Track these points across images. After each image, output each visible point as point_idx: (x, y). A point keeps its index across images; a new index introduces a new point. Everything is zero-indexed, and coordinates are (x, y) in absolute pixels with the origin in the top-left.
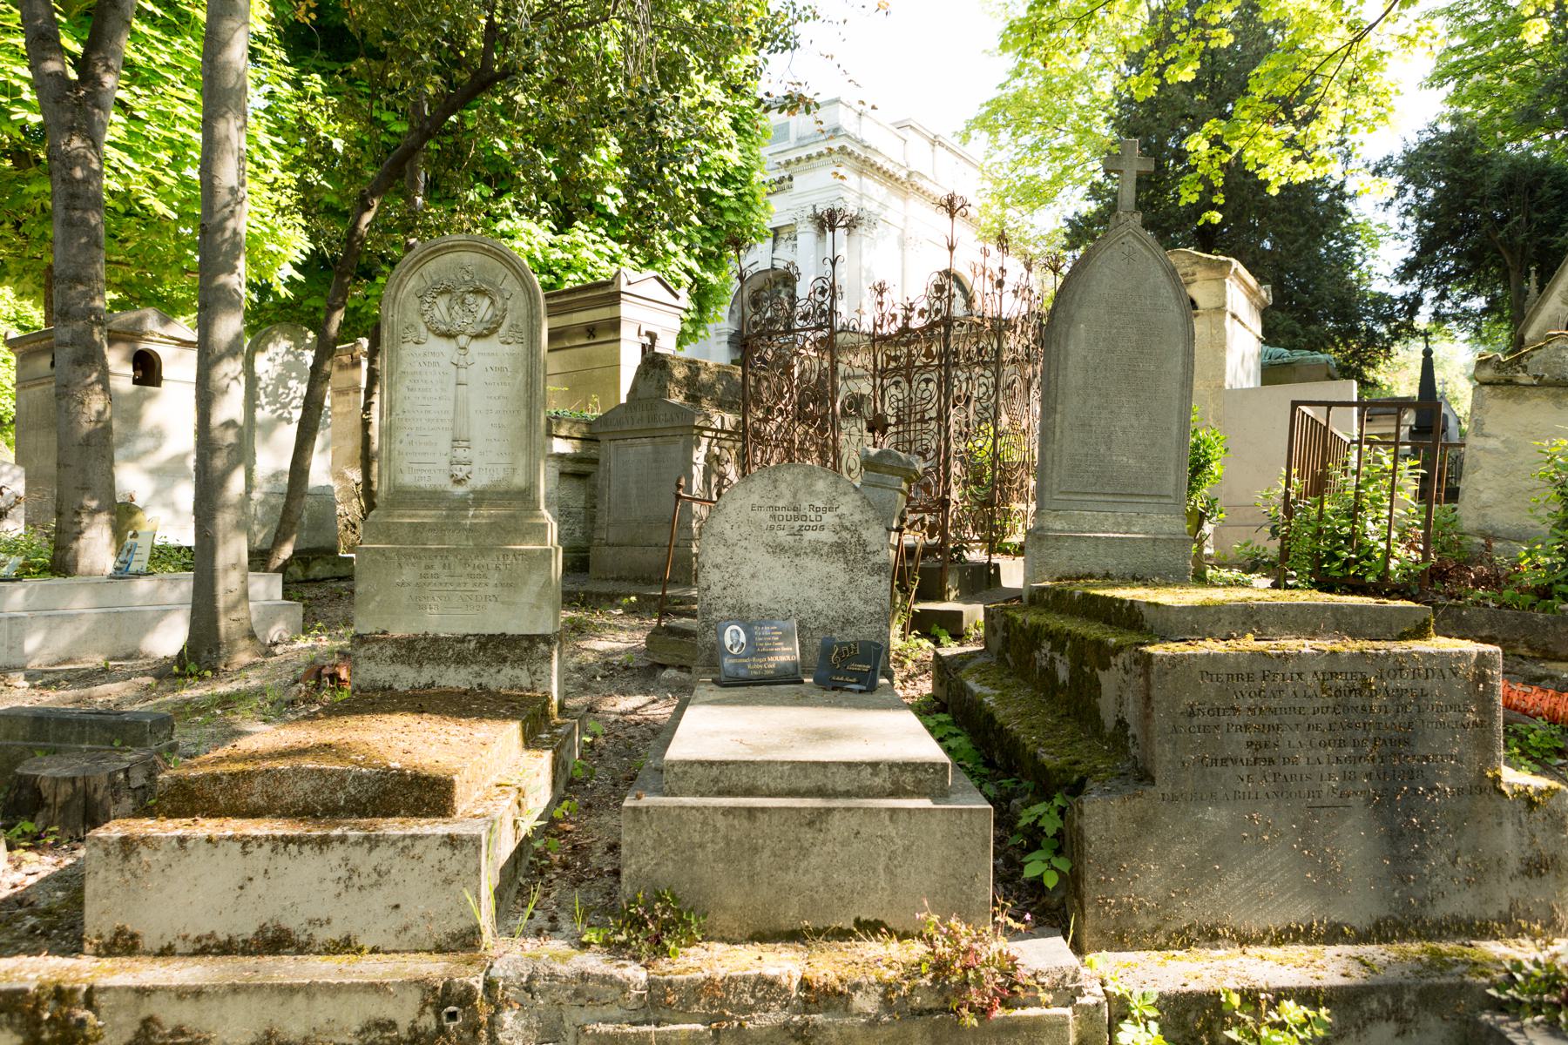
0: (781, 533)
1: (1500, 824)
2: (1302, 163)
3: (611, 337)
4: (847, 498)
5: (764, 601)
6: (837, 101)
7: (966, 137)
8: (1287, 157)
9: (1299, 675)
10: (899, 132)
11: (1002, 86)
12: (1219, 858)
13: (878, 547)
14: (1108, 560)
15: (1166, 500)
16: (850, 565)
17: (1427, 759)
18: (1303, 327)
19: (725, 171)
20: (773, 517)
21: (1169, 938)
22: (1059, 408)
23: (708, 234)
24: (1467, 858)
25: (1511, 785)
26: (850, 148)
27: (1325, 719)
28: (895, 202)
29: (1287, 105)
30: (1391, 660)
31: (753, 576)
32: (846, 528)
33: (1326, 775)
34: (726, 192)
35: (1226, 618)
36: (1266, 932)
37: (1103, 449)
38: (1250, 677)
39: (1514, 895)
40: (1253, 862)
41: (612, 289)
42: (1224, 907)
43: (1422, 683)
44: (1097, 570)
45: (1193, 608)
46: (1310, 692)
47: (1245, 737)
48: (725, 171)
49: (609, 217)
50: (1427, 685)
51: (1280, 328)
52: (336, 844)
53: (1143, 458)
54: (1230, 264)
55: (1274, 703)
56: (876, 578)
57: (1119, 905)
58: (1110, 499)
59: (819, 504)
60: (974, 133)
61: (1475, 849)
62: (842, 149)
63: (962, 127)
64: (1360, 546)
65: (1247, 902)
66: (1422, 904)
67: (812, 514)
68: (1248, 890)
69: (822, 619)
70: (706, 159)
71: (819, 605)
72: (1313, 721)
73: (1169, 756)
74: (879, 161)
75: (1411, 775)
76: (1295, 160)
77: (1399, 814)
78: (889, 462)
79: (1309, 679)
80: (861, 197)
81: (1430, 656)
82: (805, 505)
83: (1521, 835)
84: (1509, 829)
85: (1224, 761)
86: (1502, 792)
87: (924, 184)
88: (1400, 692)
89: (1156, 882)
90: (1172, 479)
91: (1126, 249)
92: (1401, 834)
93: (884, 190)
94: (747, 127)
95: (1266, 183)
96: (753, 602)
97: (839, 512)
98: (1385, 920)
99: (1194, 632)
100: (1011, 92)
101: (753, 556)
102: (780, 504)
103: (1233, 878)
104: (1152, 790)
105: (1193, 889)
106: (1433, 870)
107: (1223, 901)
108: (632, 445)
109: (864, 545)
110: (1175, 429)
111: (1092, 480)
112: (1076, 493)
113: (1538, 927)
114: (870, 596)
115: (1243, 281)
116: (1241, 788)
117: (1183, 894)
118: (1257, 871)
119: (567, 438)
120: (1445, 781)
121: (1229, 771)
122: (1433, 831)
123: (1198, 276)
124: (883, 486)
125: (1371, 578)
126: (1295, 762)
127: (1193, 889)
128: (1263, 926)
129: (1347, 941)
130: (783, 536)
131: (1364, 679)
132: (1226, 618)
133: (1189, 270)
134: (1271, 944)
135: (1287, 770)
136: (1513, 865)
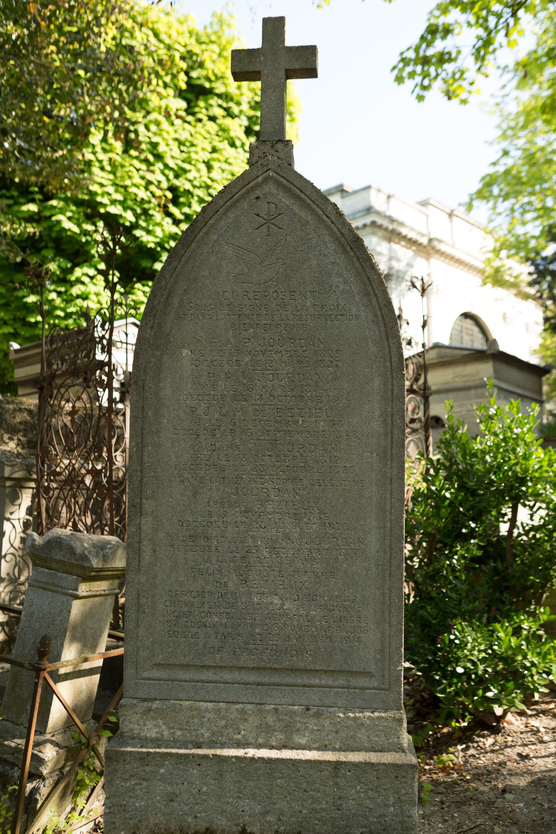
6: (369, 187)
7: (469, 207)
10: (423, 209)
11: (494, 164)
15: (361, 682)
26: (379, 221)
52: (527, 507)
58: (253, 677)
60: (476, 203)
63: (466, 199)
74: (404, 231)
78: (58, 556)
80: (391, 259)
87: (442, 247)
100: (501, 169)
112: (185, 667)
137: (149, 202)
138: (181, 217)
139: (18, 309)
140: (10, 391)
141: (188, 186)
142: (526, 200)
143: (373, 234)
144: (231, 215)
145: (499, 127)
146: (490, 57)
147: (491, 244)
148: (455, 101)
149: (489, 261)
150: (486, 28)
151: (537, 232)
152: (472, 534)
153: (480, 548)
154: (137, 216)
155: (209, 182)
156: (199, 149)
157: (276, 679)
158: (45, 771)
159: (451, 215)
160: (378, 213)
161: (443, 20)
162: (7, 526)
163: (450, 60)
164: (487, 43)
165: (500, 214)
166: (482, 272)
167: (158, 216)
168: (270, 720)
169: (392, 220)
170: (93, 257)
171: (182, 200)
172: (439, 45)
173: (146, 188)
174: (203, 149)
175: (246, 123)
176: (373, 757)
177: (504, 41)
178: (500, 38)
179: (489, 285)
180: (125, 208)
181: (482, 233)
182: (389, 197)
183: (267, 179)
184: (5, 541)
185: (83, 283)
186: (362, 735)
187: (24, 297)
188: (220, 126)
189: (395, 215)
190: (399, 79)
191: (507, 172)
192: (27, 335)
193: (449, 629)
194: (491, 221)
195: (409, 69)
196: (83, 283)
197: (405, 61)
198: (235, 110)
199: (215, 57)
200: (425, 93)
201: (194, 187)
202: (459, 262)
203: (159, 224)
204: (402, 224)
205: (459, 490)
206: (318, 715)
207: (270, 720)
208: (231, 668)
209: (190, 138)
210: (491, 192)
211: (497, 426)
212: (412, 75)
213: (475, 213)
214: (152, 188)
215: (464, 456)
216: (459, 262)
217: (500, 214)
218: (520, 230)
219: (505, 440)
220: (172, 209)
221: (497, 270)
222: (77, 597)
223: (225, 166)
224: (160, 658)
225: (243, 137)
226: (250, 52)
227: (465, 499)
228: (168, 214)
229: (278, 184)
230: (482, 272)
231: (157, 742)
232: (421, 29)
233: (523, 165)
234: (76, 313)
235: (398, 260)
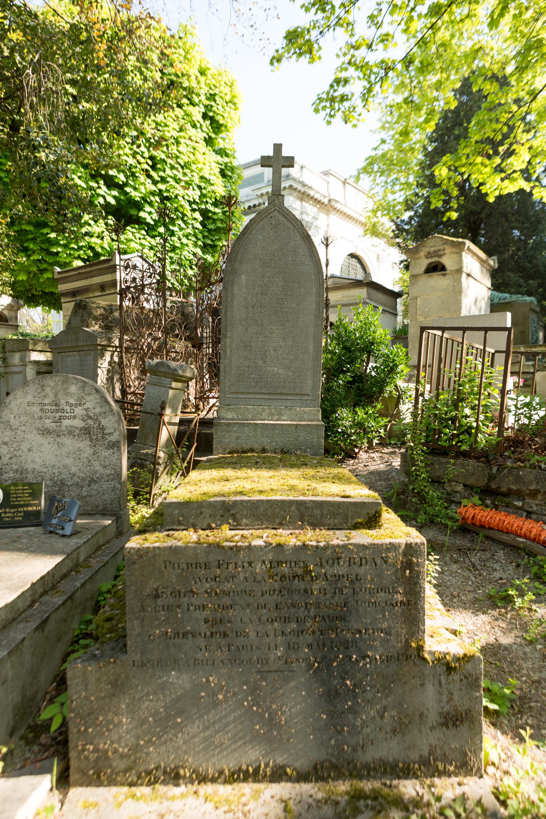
0: (47, 421)
1: (423, 685)
2: (507, 182)
3: (112, 291)
4: (91, 397)
5: (37, 466)
7: (358, 178)
8: (497, 178)
9: (250, 564)
10: (325, 177)
11: (375, 149)
12: (180, 713)
13: (112, 430)
14: (264, 439)
15: (305, 398)
16: (94, 443)
17: (360, 632)
18: (526, 281)
19: (216, 199)
20: (42, 410)
21: (139, 777)
22: (229, 334)
23: (206, 234)
24: (394, 713)
25: (432, 653)
26: (295, 186)
27: (272, 600)
28: (322, 216)
29: (495, 145)
30: (329, 552)
31: (29, 450)
32: (90, 418)
33: (272, 646)
34: (217, 210)
35: (207, 512)
36: (221, 772)
37: (260, 363)
38: (206, 566)
39: (433, 742)
40: (211, 716)
41: (112, 263)
42: (185, 753)
43: (356, 569)
44: (256, 446)
45: (179, 503)
46: (259, 578)
47: (201, 615)
48: (216, 199)
49: (148, 224)
50: (361, 571)
51: (511, 282)
53: (289, 368)
54: (464, 244)
55: (227, 586)
56: (111, 451)
57: (96, 750)
58: (267, 397)
59: (72, 401)
60: (362, 176)
61: (401, 705)
62: (291, 186)
63: (355, 173)
64: (461, 426)
65: (205, 749)
66: (355, 750)
67: (68, 408)
68: (206, 739)
69: (75, 479)
70: (204, 191)
71: (74, 470)
72: (262, 601)
73: (138, 630)
74: (312, 193)
75: (346, 645)
76: (502, 180)
77: (335, 678)
78: (162, 369)
79: (259, 568)
81: (364, 547)
82: (63, 402)
83: (441, 694)
84: (430, 689)
85: (185, 635)
86: (424, 659)
88: (338, 578)
89: (128, 732)
90: (310, 382)
91: (273, 221)
92: (337, 693)
93: (315, 209)
94: (230, 174)
95: (486, 194)
96: (30, 467)
97: (86, 406)
98: (322, 764)
99: (179, 523)
100: (380, 152)
101: (29, 436)
102: (47, 401)
103: (194, 728)
104: (124, 657)
105: (159, 738)
106: (364, 722)
107: (184, 748)
108: (69, 356)
109: (103, 429)
110: (311, 348)
111: (253, 384)
112: (242, 393)
113: (452, 768)
114: (107, 463)
115: (474, 254)
116: (200, 656)
117: (149, 742)
118: (213, 724)
119: (40, 351)
120: (376, 651)
121: (190, 641)
122: (364, 691)
123: (446, 251)
124: (160, 385)
125: (464, 448)
126: (247, 635)
127: (159, 738)
128: (219, 767)
129: (290, 779)
130: (48, 423)
131: (306, 566)
132: (207, 512)
133: (442, 247)
134: (225, 782)
135: (239, 642)
136: (433, 717)
137: (136, 167)
138: (159, 179)
139: (42, 242)
140: (33, 301)
141: (163, 156)
142: (395, 176)
143: (290, 194)
144: (261, 224)
145: (380, 120)
146: (370, 99)
147: (371, 205)
148: (349, 125)
149: (369, 217)
150: (369, 82)
151: (401, 200)
152: (348, 370)
153: (351, 377)
154: (127, 177)
155: (178, 154)
156: (170, 129)
157: (276, 397)
158: (161, 462)
159: (344, 183)
160: (294, 179)
161: (343, 75)
162: (99, 371)
163: (347, 99)
164: (370, 90)
165: (378, 184)
166: (364, 225)
167: (142, 178)
168: (273, 411)
169: (304, 185)
170: (96, 206)
171: (159, 166)
172: (341, 90)
173: (134, 157)
174: (174, 129)
175: (203, 110)
176: (309, 423)
177: (380, 91)
178: (377, 88)
179: (368, 236)
180: (119, 171)
181: (365, 197)
182: (302, 167)
183: (275, 210)
184: (99, 379)
185: (89, 225)
186: (305, 416)
187: (48, 234)
188: (185, 111)
189: (306, 181)
190: (316, 111)
191: (383, 155)
192: (51, 261)
193: (335, 412)
194: (372, 189)
195: (323, 104)
196: (89, 225)
197: (320, 100)
198: (196, 99)
199: (182, 58)
200: (332, 120)
201: (168, 157)
202: (349, 217)
203: (142, 184)
204: (311, 188)
205: (342, 349)
206: (290, 409)
207: (273, 411)
208: (259, 393)
209: (164, 120)
210: (373, 169)
211: (362, 318)
212: (324, 108)
213: (361, 183)
214: (139, 157)
215: (346, 332)
216: (349, 217)
217: (378, 184)
218: (390, 197)
219: (365, 324)
220: (153, 173)
221: (374, 226)
222: (172, 388)
223: (189, 142)
224: (233, 390)
225: (201, 120)
226: (269, 157)
227: (345, 353)
228: (149, 176)
229: (279, 212)
230: (364, 225)
231: (232, 419)
232: (331, 80)
233: (394, 151)
234: (85, 246)
235: (307, 214)
